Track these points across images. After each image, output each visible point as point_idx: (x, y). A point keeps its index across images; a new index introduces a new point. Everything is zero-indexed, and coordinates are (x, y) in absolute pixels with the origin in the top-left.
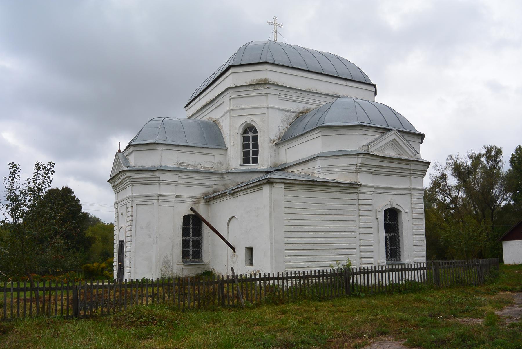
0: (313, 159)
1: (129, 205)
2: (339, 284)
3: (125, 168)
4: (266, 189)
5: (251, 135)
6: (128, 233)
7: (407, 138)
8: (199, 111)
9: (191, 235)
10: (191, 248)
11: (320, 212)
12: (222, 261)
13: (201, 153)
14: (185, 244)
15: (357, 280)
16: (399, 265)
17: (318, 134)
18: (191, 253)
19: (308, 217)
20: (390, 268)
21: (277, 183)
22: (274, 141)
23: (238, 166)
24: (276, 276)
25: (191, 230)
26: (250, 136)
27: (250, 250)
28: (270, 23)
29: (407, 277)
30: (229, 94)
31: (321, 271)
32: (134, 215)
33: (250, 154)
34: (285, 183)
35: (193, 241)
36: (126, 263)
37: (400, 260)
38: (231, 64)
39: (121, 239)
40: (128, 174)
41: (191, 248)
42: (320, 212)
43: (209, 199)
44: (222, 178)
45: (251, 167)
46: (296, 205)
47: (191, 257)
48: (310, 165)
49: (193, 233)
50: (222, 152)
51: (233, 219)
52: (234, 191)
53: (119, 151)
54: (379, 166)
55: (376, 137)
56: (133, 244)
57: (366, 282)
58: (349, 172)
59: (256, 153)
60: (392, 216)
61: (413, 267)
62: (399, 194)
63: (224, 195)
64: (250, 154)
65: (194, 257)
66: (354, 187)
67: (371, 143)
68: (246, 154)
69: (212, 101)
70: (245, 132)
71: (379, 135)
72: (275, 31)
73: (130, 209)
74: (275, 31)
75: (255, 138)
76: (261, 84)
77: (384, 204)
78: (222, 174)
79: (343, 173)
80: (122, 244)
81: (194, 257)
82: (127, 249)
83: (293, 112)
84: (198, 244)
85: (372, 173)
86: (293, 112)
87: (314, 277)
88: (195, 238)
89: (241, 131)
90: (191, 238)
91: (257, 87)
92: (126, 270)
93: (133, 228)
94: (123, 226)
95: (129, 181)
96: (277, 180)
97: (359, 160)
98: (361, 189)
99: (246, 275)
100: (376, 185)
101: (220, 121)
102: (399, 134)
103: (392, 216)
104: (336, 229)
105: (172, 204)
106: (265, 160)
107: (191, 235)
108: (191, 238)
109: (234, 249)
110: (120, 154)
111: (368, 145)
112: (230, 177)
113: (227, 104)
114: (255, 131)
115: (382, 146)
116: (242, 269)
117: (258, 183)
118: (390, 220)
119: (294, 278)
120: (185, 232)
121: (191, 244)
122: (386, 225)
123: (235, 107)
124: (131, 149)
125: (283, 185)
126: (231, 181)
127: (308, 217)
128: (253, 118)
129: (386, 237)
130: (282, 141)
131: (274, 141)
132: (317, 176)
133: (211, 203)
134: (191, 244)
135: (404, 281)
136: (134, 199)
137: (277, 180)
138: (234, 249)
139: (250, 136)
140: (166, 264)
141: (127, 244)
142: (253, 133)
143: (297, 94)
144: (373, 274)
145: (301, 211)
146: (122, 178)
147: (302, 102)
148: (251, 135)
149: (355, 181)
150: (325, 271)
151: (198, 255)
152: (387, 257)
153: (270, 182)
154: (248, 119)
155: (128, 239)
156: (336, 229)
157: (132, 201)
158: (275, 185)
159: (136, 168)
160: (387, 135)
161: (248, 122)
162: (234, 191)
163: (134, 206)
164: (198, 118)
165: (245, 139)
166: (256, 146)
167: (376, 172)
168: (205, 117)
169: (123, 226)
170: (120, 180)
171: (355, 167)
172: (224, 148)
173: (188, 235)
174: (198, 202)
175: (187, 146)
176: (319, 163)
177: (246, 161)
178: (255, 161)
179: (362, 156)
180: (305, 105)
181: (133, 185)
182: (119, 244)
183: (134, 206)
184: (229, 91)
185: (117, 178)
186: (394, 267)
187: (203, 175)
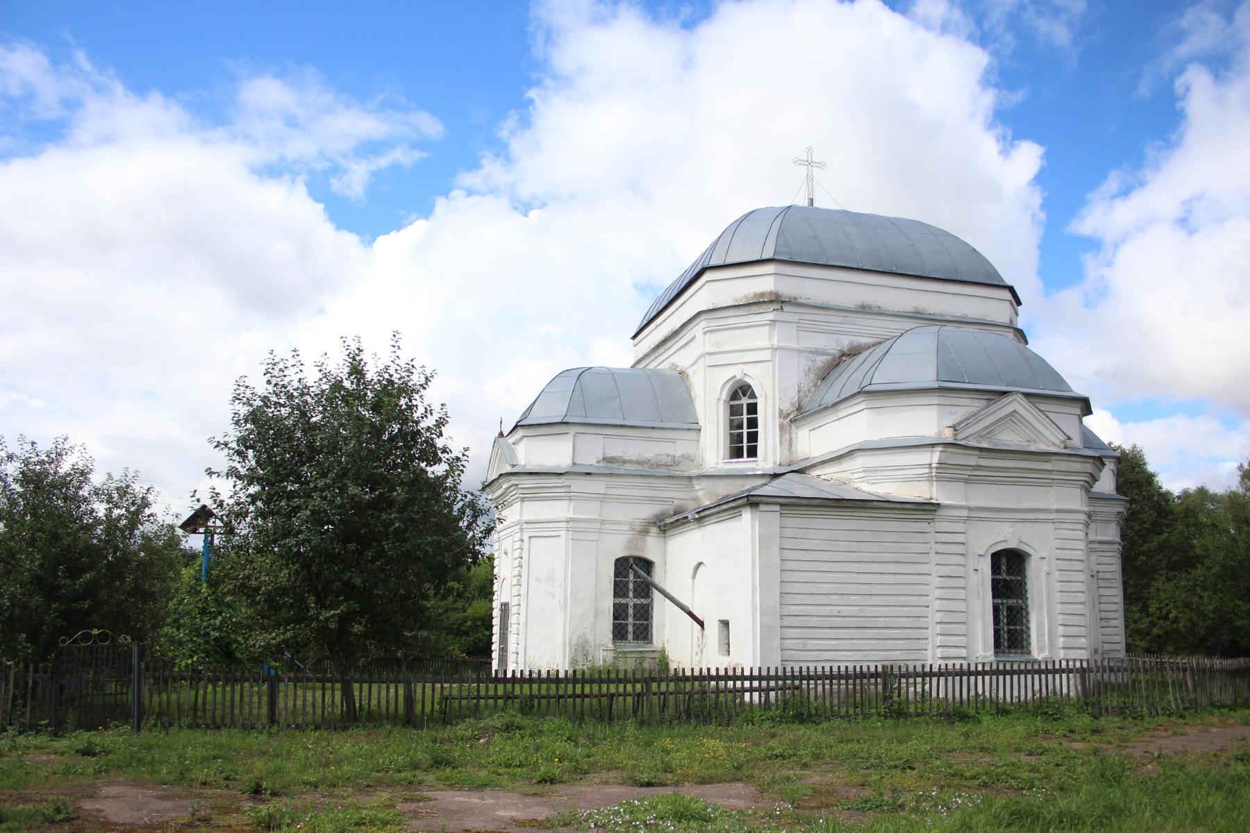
0: (850, 453)
1: (517, 537)
2: (881, 697)
3: (508, 469)
4: (747, 514)
5: (745, 401)
6: (515, 590)
7: (1043, 407)
8: (658, 346)
9: (631, 594)
10: (631, 620)
11: (854, 557)
12: (682, 646)
13: (648, 438)
14: (619, 612)
15: (912, 689)
16: (1012, 663)
17: (860, 405)
18: (630, 629)
19: (827, 567)
20: (1001, 667)
21: (768, 504)
22: (789, 415)
23: (720, 462)
24: (772, 673)
25: (631, 586)
26: (742, 404)
27: (725, 624)
28: (798, 162)
29: (1037, 688)
30: (702, 325)
31: (812, 669)
32: (525, 555)
33: (743, 442)
34: (781, 505)
35: (635, 606)
36: (512, 647)
37: (1029, 653)
38: (706, 265)
39: (504, 601)
40: (514, 480)
41: (631, 620)
42: (854, 557)
43: (668, 523)
44: (692, 486)
45: (744, 464)
46: (804, 544)
47: (630, 637)
48: (847, 465)
49: (635, 590)
50: (692, 435)
51: (702, 567)
52: (702, 514)
53: (501, 434)
54: (979, 467)
55: (975, 410)
56: (523, 609)
57: (1001, 695)
58: (917, 478)
59: (753, 437)
60: (1009, 569)
61: (1057, 667)
62: (1024, 521)
63: (684, 521)
64: (743, 442)
65: (636, 638)
66: (927, 509)
67: (960, 423)
68: (736, 439)
69: (675, 334)
70: (734, 396)
71: (982, 404)
72: (810, 178)
73: (517, 545)
74: (810, 178)
75: (753, 409)
76: (764, 302)
77: (991, 542)
78: (690, 478)
79: (906, 480)
80: (505, 608)
81: (636, 638)
82: (513, 619)
83: (828, 354)
84: (644, 613)
85: (966, 481)
86: (828, 354)
87: (872, 675)
88: (638, 601)
89: (725, 395)
90: (631, 601)
91: (755, 309)
92: (511, 658)
93: (524, 581)
94: (508, 576)
95: (516, 494)
96: (765, 499)
97: (935, 457)
98: (941, 512)
99: (709, 670)
100: (973, 504)
101: (690, 372)
102: (1024, 401)
103: (1009, 569)
104: (887, 590)
105: (593, 536)
106: (769, 454)
107: (631, 594)
108: (631, 601)
109: (701, 624)
110: (501, 440)
111: (954, 427)
112: (705, 484)
113: (700, 340)
114: (753, 396)
115: (986, 427)
116: (714, 661)
117: (733, 504)
118: (1009, 572)
119: (1063, 671)
120: (620, 589)
121: (631, 611)
122: (995, 583)
123: (714, 349)
124: (520, 433)
125: (777, 508)
126: (705, 494)
127: (827, 567)
128: (748, 369)
129: (996, 609)
130: (799, 414)
131: (789, 415)
132: (857, 485)
133: (668, 533)
134: (631, 611)
135: (858, 695)
136: (525, 526)
137: (765, 499)
138: (701, 624)
139: (742, 404)
140: (581, 648)
141: (513, 610)
142: (750, 397)
143: (835, 318)
144: (1029, 677)
145: (815, 556)
146: (505, 486)
147: (847, 333)
148: (745, 401)
149: (928, 496)
150: (804, 669)
151: (644, 633)
152: (997, 644)
153: (753, 502)
154: (736, 372)
155: (515, 601)
156: (887, 590)
157: (522, 529)
158: (762, 507)
159: (529, 469)
160: (1000, 404)
161: (738, 377)
162: (702, 514)
163: (526, 538)
164: (651, 366)
165: (734, 411)
166: (753, 423)
167: (972, 477)
168: (662, 363)
169: (508, 576)
170: (501, 491)
171: (927, 471)
172: (695, 426)
173: (626, 595)
174: (645, 532)
175: (622, 426)
176: (860, 462)
177: (736, 453)
178: (753, 452)
179: (939, 449)
180: (854, 338)
181: (523, 500)
182: (501, 610)
183: (526, 538)
184: (703, 317)
185: (496, 485)
186: (1008, 667)
187: (650, 480)
